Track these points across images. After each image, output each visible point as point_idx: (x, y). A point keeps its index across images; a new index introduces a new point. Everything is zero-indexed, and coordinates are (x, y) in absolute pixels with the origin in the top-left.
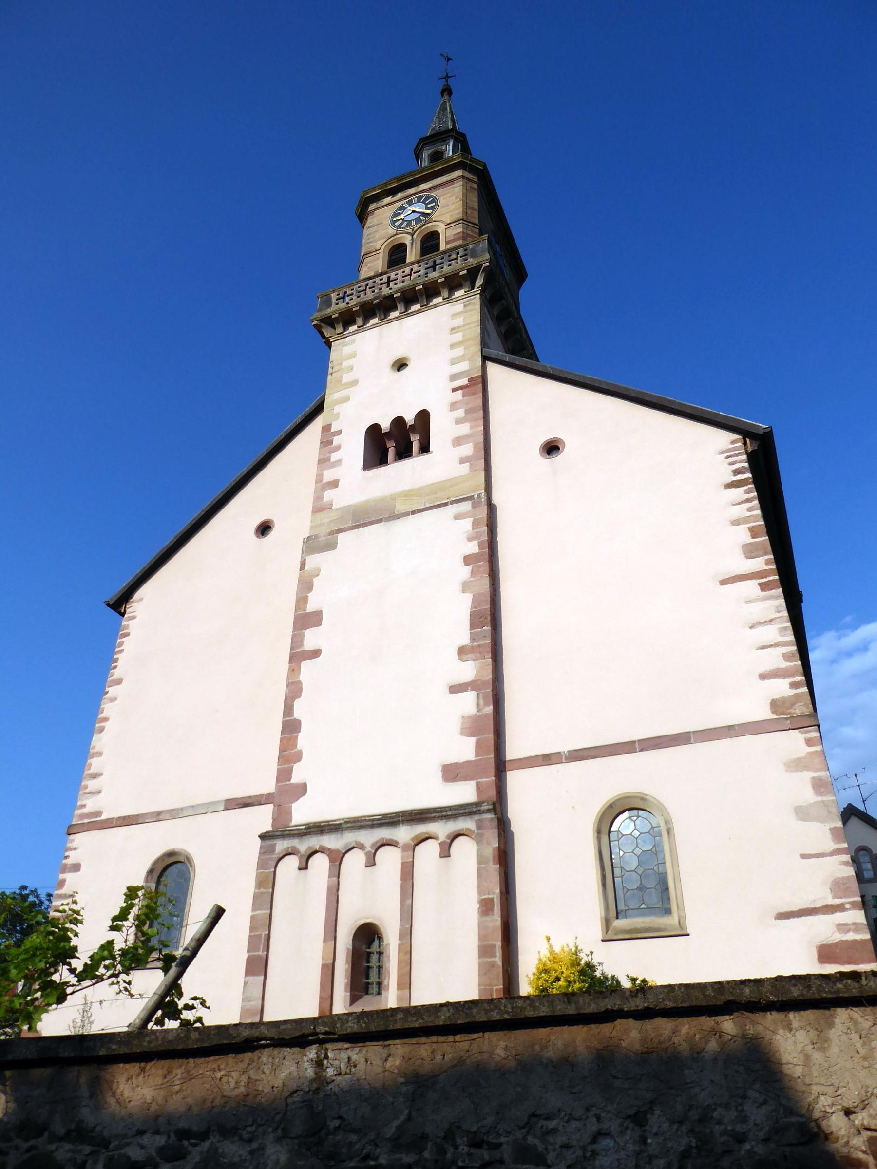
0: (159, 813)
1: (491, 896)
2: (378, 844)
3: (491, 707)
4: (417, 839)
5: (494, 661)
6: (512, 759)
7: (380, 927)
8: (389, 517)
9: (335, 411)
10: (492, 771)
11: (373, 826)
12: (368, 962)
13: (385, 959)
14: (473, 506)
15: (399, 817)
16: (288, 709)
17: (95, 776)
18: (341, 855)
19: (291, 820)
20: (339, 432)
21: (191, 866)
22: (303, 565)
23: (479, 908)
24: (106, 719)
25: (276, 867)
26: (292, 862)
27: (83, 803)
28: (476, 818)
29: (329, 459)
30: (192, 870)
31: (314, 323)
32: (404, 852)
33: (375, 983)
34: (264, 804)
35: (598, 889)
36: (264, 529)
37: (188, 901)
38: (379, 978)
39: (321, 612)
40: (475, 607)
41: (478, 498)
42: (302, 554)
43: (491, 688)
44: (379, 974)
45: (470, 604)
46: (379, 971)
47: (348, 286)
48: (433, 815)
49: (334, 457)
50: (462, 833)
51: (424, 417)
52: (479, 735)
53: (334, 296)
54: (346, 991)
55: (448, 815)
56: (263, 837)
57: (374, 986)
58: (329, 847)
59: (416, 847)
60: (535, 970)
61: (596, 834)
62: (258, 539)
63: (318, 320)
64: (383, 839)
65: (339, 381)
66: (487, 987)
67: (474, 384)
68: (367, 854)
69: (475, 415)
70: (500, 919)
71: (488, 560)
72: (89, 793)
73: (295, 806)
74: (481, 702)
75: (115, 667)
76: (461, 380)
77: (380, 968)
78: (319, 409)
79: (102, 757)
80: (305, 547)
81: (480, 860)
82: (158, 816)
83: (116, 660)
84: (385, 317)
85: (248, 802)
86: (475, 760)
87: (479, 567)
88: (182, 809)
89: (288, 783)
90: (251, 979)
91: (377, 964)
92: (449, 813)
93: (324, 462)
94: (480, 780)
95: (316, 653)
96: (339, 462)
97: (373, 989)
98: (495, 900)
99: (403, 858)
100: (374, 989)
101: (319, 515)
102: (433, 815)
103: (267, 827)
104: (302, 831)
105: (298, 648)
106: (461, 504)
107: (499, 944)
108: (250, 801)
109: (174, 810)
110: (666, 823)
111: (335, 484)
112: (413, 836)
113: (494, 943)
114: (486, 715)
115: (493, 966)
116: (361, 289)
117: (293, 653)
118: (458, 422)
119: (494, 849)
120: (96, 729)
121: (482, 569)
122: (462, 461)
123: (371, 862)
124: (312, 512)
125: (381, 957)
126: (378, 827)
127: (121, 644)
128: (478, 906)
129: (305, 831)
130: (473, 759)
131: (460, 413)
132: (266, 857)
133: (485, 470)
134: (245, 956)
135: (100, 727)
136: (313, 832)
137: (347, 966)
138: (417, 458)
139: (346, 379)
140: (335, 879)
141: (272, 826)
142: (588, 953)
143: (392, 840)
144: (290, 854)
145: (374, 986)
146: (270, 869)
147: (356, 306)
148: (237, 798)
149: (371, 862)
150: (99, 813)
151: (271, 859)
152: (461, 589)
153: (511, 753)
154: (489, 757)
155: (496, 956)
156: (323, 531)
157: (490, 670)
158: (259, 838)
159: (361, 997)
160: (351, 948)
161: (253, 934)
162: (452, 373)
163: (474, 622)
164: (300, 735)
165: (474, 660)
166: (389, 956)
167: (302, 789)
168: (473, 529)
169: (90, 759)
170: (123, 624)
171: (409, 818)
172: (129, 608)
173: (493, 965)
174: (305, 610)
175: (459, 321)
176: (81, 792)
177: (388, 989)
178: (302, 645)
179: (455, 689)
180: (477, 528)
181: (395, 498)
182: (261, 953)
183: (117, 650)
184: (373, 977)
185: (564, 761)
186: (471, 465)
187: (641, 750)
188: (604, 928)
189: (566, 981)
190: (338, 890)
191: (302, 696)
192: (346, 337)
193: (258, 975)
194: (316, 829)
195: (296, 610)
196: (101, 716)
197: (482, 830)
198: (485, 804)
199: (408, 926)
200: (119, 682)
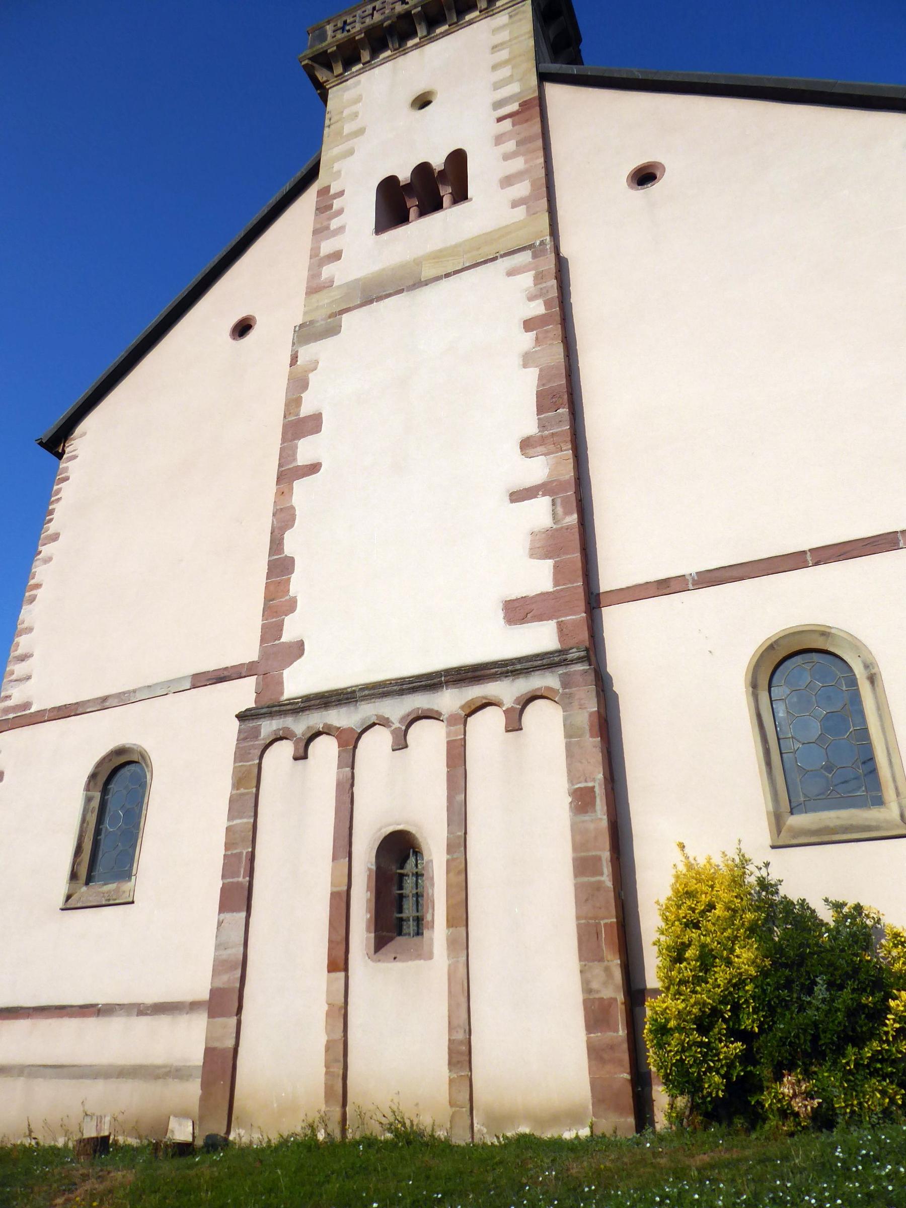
0: (105, 699)
1: (590, 784)
2: (411, 718)
3: (575, 516)
4: (470, 707)
5: (576, 457)
6: (609, 590)
7: (418, 836)
8: (414, 285)
9: (335, 169)
10: (582, 604)
11: (401, 692)
12: (401, 887)
13: (427, 883)
14: (535, 256)
15: (441, 677)
16: (276, 544)
17: (23, 658)
18: (356, 736)
19: (282, 693)
20: (341, 193)
21: (147, 766)
22: (294, 359)
23: (571, 803)
24: (38, 586)
25: (261, 757)
26: (284, 750)
27: (8, 693)
28: (561, 672)
29: (327, 228)
30: (148, 771)
31: (303, 63)
32: (451, 726)
33: (411, 919)
34: (245, 677)
35: (760, 772)
36: (243, 328)
37: (144, 812)
38: (418, 911)
39: (320, 415)
40: (543, 385)
41: (540, 244)
42: (292, 346)
43: (574, 490)
44: (417, 905)
45: (536, 382)
46: (417, 902)
47: (347, 13)
48: (493, 671)
49: (335, 224)
50: (539, 694)
51: (458, 159)
52: (558, 556)
53: (329, 28)
54: (368, 931)
55: (517, 670)
56: (242, 717)
57: (411, 922)
58: (338, 725)
59: (469, 719)
60: (670, 893)
61: (751, 689)
62: (234, 342)
63: (308, 59)
64: (418, 708)
65: (340, 133)
66: (591, 921)
67: (528, 109)
68: (394, 733)
69: (531, 146)
70: (605, 817)
71: (560, 322)
72: (16, 680)
73: (286, 673)
74: (560, 510)
75: (51, 520)
76: (511, 106)
77: (418, 896)
78: (312, 174)
79: (33, 633)
80: (297, 336)
81: (570, 732)
82: (103, 703)
83: (51, 512)
84: (400, 46)
85: (222, 675)
86: (554, 591)
87: (547, 331)
88: (134, 691)
89: (277, 642)
90: (227, 916)
91: (414, 891)
92: (518, 667)
93: (320, 232)
94: (563, 619)
95: (314, 468)
96: (341, 229)
97: (409, 927)
98: (597, 790)
99: (448, 734)
100: (411, 926)
101: (316, 296)
102: (493, 671)
103: (249, 702)
104: (297, 706)
105: (288, 464)
106: (516, 256)
107: (606, 855)
108: (226, 673)
109: (124, 693)
110: (866, 666)
111: (336, 256)
112: (463, 702)
113: (598, 853)
114: (567, 528)
115: (598, 889)
116: (367, 13)
117: (282, 472)
118: (507, 157)
119: (591, 714)
120: (25, 599)
121: (551, 335)
122: (515, 204)
123: (401, 743)
124: (306, 294)
125: (420, 881)
126: (409, 693)
127: (58, 491)
128: (570, 799)
129: (302, 705)
130: (551, 590)
131: (511, 146)
132: (246, 744)
133: (549, 213)
134: (220, 884)
135: (30, 596)
136: (314, 705)
137: (369, 893)
138: (450, 210)
139: (348, 128)
140: (348, 769)
141: (256, 702)
142: (761, 865)
143: (431, 710)
144: (281, 739)
145: (411, 922)
146: (253, 760)
147: (360, 32)
148: (208, 672)
149: (401, 743)
150: (27, 705)
151: (253, 747)
152: (521, 363)
153: (607, 581)
154: (575, 585)
155: (602, 874)
156: (320, 315)
157: (571, 466)
158: (236, 719)
159: (391, 939)
160: (374, 867)
161: (229, 853)
162: (495, 100)
163: (545, 401)
164: (293, 576)
165: (545, 455)
166: (432, 878)
167: (298, 649)
168: (535, 285)
169: (17, 637)
170: (61, 467)
171: (455, 678)
172: (68, 446)
173: (598, 887)
174: (298, 415)
175: (504, 36)
176: (5, 680)
177: (433, 927)
178: (295, 460)
179: (518, 496)
180: (541, 283)
181: (421, 262)
182: (242, 879)
183: (53, 499)
184: (408, 909)
185: (691, 587)
186: (528, 208)
187: (816, 564)
188: (774, 826)
189: (728, 909)
190: (352, 785)
191: (296, 525)
192: (347, 80)
193: (238, 910)
194: (318, 701)
195: (285, 417)
196: (32, 582)
197: (570, 688)
198: (574, 650)
199: (461, 833)
200: (55, 537)
